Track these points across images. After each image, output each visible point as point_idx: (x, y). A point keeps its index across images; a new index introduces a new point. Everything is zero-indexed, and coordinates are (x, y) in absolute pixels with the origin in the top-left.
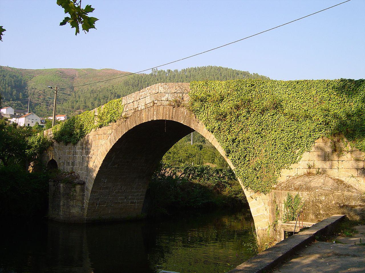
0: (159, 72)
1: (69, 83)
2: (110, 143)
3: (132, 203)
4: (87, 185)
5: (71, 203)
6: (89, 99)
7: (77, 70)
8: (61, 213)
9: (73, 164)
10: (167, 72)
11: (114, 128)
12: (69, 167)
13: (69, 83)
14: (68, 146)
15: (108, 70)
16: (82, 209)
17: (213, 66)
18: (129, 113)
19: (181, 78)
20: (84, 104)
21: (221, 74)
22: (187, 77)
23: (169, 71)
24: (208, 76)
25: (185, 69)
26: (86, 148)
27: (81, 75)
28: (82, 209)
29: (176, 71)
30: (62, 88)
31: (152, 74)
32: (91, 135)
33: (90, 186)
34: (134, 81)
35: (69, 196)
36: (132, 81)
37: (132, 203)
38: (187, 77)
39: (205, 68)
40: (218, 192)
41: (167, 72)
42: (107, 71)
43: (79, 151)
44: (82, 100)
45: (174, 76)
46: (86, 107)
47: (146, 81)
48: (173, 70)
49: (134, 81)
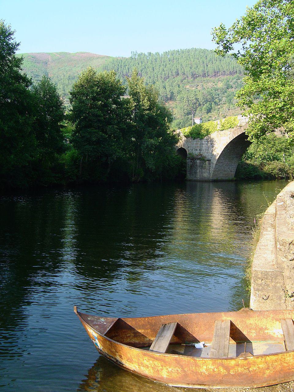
0: (139, 55)
1: (43, 69)
2: (229, 138)
3: (231, 171)
4: (212, 161)
5: (204, 171)
6: (67, 86)
7: (49, 54)
8: (198, 176)
9: (200, 150)
10: (148, 55)
11: (232, 131)
12: (197, 152)
13: (43, 69)
14: (195, 140)
15: (84, 53)
16: (210, 174)
17: (197, 48)
18: (242, 124)
19: (164, 62)
20: (63, 92)
21: (206, 57)
22: (170, 61)
23: (150, 54)
24: (192, 60)
25: (167, 52)
26: (211, 142)
27: (54, 59)
28: (210, 174)
29: (157, 54)
30: (36, 74)
31: (132, 58)
32: (213, 135)
33: (215, 162)
34: (113, 66)
35: (202, 167)
36: (111, 66)
37: (231, 171)
38: (170, 61)
39: (189, 51)
40: (262, 169)
41: (148, 55)
42: (82, 55)
43: (205, 143)
44: (61, 87)
45: (156, 60)
46: (65, 94)
47: (126, 66)
48: (154, 53)
49: (113, 66)
